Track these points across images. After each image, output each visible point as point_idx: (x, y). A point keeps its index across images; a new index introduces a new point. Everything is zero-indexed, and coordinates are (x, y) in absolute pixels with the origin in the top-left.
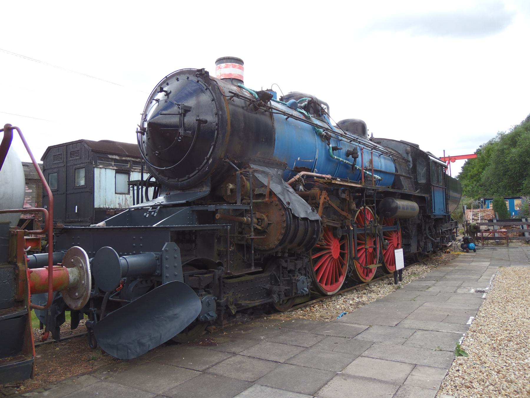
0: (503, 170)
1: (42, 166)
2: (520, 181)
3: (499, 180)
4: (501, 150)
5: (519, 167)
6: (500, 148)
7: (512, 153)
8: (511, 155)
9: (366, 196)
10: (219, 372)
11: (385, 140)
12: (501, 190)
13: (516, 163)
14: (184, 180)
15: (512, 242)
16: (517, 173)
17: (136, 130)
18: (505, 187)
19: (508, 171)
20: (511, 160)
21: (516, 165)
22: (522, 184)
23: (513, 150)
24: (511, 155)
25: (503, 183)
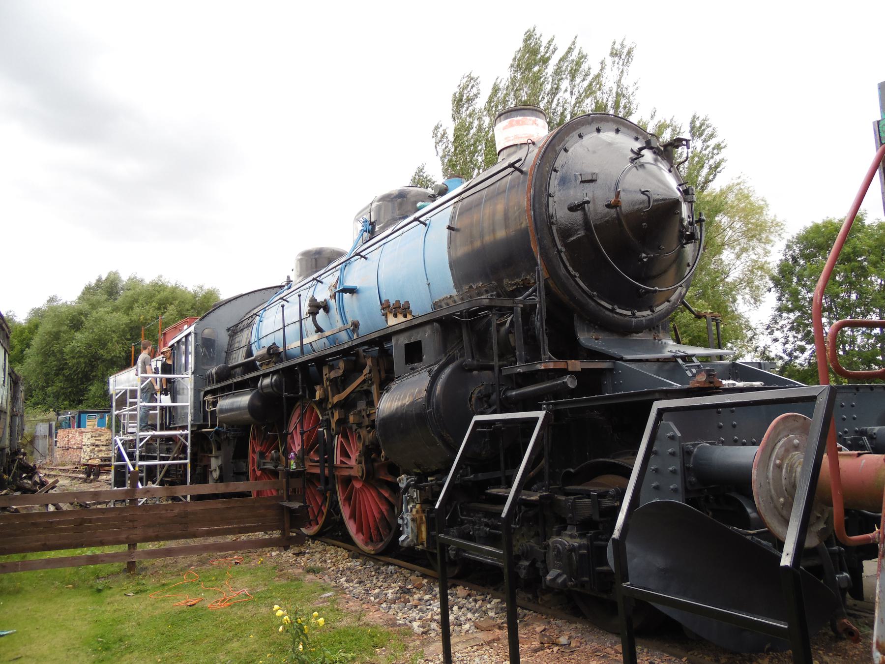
0: (56, 366)
1: (66, 383)
2: (81, 387)
3: (48, 383)
4: (54, 332)
5: (85, 363)
6: (54, 330)
7: (76, 339)
8: (74, 343)
9: (491, 368)
10: (278, 552)
11: (652, 466)
12: (50, 400)
13: (79, 357)
14: (543, 339)
15: (870, 247)
16: (78, 373)
17: (436, 125)
18: (57, 396)
19: (63, 369)
20: (72, 351)
21: (82, 360)
22: (86, 390)
23: (78, 335)
24: (74, 343)
25: (54, 387)
